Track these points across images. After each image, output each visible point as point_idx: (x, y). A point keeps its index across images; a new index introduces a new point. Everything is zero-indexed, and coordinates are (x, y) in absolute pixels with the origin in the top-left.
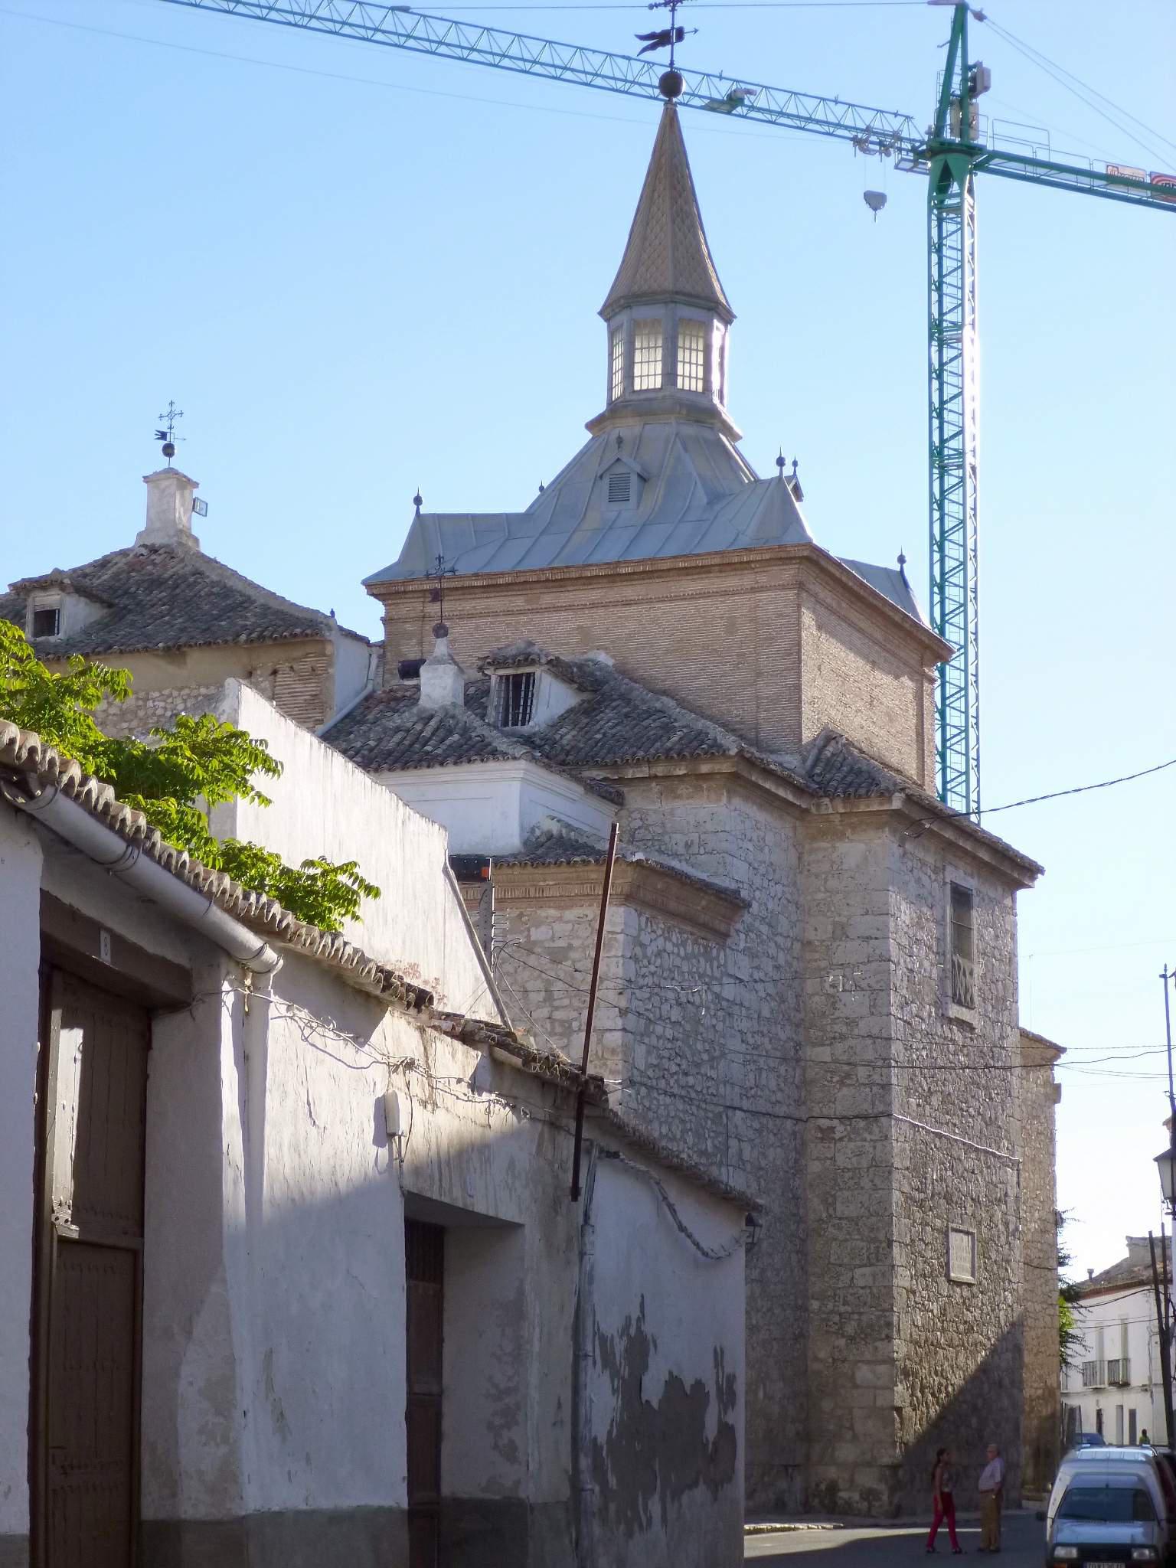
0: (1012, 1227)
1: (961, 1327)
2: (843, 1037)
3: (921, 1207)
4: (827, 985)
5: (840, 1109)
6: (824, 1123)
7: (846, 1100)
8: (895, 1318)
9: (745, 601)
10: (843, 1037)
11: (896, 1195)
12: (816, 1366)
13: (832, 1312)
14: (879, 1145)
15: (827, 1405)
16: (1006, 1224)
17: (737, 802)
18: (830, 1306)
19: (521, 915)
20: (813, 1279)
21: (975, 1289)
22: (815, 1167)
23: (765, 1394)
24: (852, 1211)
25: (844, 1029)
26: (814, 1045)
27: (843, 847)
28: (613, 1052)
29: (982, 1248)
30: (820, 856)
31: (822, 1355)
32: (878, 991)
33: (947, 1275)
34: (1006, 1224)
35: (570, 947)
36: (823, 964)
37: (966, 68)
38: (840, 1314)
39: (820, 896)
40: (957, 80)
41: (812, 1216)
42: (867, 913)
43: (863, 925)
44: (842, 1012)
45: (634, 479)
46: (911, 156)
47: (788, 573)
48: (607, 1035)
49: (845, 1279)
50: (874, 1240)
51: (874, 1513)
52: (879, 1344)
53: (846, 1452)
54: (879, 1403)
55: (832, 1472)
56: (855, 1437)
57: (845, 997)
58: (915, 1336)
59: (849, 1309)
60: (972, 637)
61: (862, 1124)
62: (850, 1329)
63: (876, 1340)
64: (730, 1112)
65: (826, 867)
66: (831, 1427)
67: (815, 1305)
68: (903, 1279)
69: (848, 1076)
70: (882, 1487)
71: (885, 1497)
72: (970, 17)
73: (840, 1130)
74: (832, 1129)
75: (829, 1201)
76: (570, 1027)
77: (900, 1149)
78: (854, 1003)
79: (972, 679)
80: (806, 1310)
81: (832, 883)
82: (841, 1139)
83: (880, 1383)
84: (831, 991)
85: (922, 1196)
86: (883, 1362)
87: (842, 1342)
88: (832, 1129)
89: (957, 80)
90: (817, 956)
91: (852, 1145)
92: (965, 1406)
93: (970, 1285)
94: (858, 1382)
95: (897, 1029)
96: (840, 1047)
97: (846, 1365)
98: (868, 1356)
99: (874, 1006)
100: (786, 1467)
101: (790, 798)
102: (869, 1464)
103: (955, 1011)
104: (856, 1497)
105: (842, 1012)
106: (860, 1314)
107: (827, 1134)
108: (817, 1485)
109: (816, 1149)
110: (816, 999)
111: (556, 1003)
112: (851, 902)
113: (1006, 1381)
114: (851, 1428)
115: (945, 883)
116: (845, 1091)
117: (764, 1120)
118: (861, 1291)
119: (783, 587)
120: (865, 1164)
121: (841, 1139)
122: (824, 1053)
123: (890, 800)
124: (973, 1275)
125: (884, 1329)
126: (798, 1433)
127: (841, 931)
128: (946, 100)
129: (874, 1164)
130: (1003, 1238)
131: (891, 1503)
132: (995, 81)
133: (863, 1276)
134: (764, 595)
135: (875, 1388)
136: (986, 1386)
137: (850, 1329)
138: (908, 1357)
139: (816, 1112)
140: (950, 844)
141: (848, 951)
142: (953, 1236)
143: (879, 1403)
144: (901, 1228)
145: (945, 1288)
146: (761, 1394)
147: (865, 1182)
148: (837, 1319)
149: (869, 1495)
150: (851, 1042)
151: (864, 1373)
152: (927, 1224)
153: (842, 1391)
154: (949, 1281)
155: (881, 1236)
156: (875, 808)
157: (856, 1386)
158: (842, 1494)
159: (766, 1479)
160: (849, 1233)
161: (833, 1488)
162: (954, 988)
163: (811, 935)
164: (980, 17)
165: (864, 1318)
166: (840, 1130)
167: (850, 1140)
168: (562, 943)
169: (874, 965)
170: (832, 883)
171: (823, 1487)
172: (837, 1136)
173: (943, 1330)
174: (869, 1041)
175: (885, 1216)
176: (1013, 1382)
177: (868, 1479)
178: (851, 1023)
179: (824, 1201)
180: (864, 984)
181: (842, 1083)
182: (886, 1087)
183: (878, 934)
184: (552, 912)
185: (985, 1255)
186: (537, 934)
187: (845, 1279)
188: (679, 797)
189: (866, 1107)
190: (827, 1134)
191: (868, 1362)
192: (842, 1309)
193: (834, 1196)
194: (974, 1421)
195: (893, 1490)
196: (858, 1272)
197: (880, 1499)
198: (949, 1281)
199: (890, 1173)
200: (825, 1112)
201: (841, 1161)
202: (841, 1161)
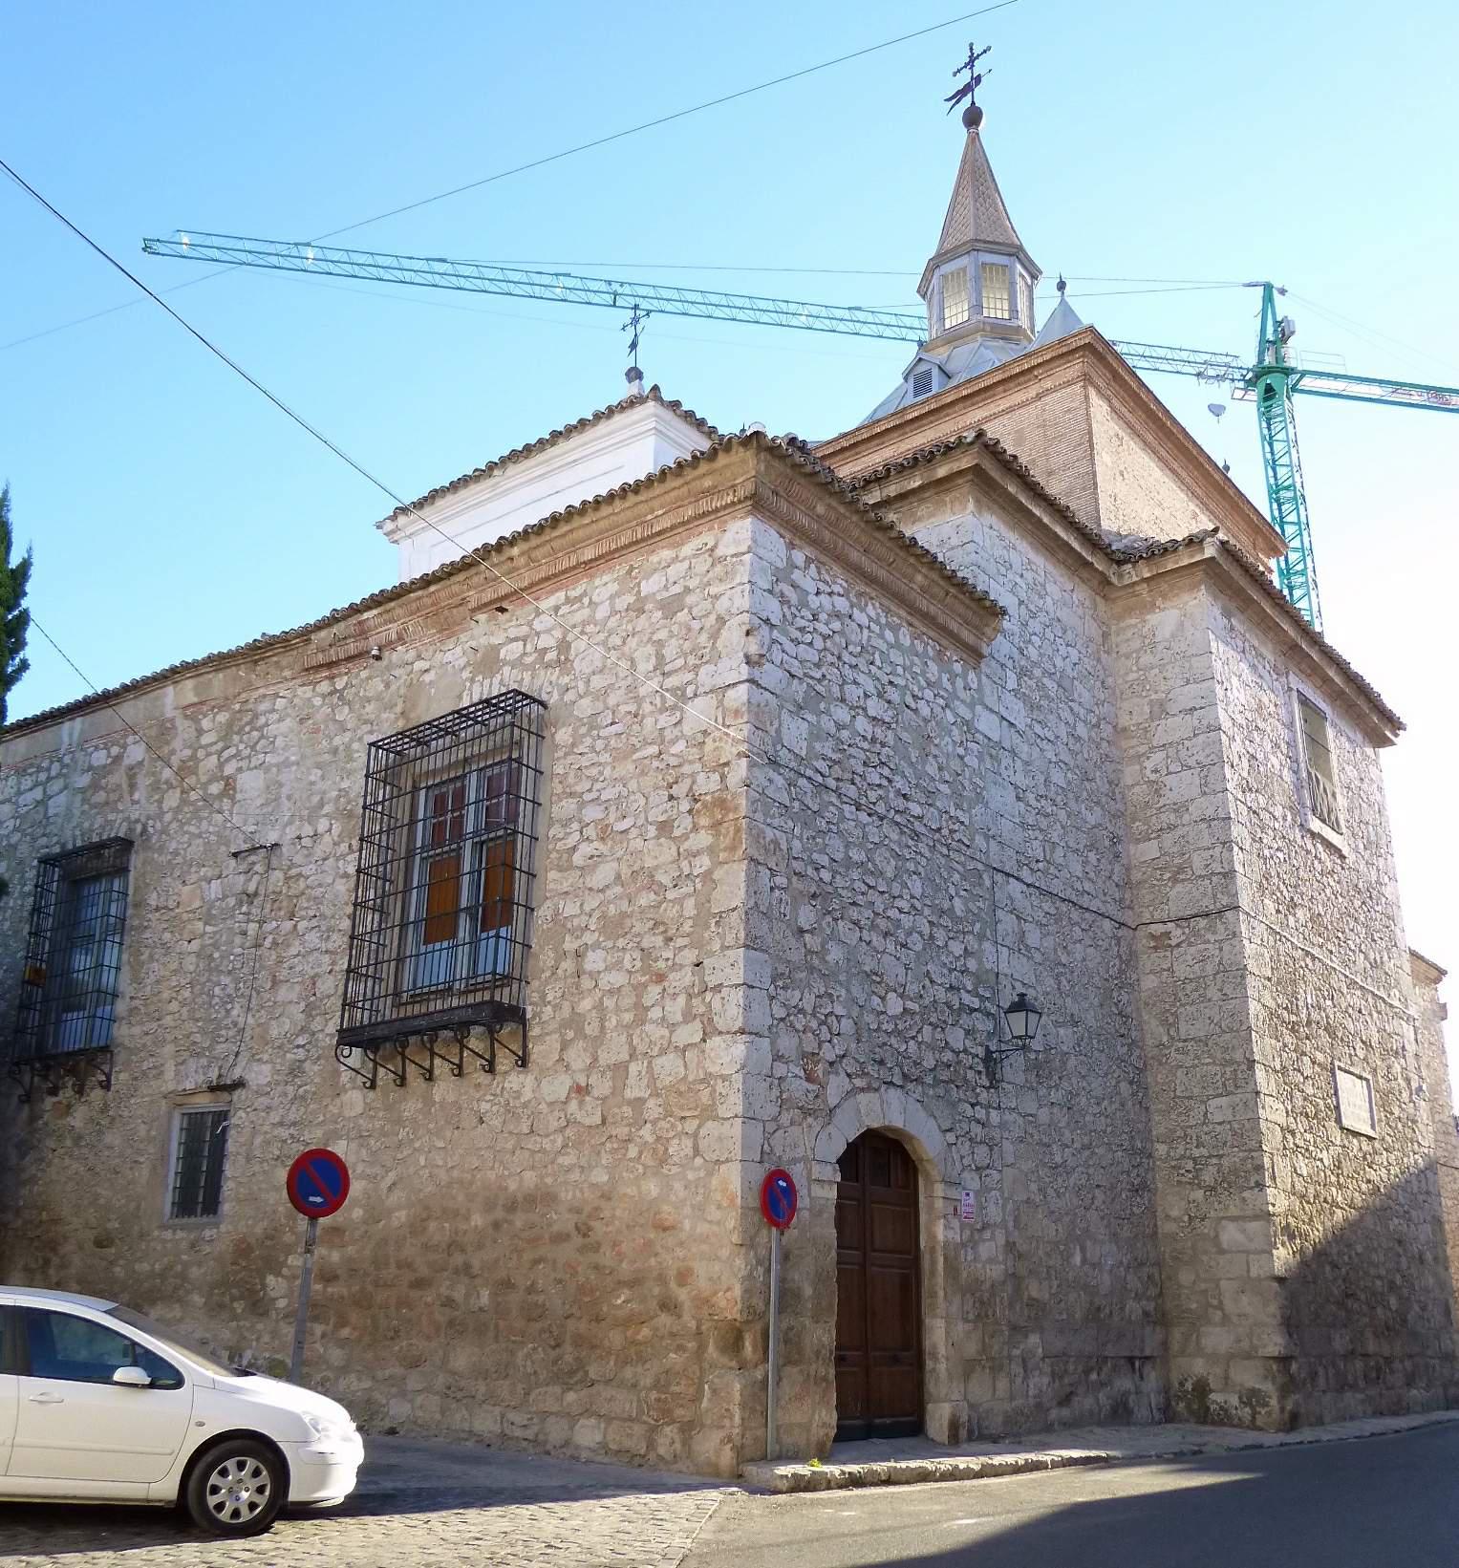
0: (1414, 1085)
1: (1364, 1187)
2: (1171, 827)
3: (1293, 1030)
4: (1148, 772)
5: (1174, 909)
6: (1157, 929)
7: (1180, 898)
8: (1266, 1160)
9: (1032, 410)
10: (1171, 827)
11: (1253, 1007)
12: (1169, 1227)
13: (1183, 1157)
14: (1226, 947)
15: (1185, 1277)
16: (1408, 1080)
17: (990, 519)
18: (1181, 1151)
19: (632, 568)
20: (1157, 1118)
21: (1377, 1145)
22: (1149, 983)
23: (1084, 1261)
24: (1199, 1030)
25: (1172, 817)
26: (1138, 841)
27: (1153, 619)
28: (737, 713)
29: (1382, 1100)
30: (1129, 634)
31: (1175, 1213)
32: (1210, 768)
33: (1339, 1120)
34: (1408, 1080)
35: (687, 590)
36: (1142, 749)
37: (1277, 323)
38: (1194, 1160)
39: (1133, 676)
40: (1270, 329)
41: (1150, 1042)
42: (1188, 682)
43: (1186, 696)
44: (1169, 797)
45: (935, 372)
46: (1241, 384)
47: (1075, 368)
48: (730, 693)
49: (1196, 1116)
50: (1231, 1062)
51: (1259, 1423)
52: (1246, 1194)
53: (1217, 1339)
54: (1254, 1273)
55: (1199, 1367)
56: (1226, 1319)
57: (1170, 781)
58: (1298, 1187)
59: (1204, 1152)
60: (1302, 526)
61: (1203, 923)
62: (1208, 1176)
63: (1243, 1189)
64: (999, 877)
65: (1136, 644)
66: (1194, 1306)
67: (1161, 1149)
68: (1273, 1112)
69: (1181, 869)
70: (1268, 1387)
71: (1274, 1402)
72: (1275, 293)
73: (1177, 934)
74: (1167, 935)
75: (1170, 1021)
76: (684, 694)
77: (1255, 950)
78: (1181, 786)
79: (1306, 552)
80: (1150, 1156)
81: (1146, 659)
82: (1178, 945)
83: (1252, 1246)
84: (1153, 777)
85: (1294, 1018)
86: (1256, 1218)
87: (1199, 1195)
88: (1167, 935)
89: (1270, 329)
90: (1134, 742)
91: (1192, 950)
92: (1378, 1283)
93: (1370, 1138)
94: (1225, 1246)
95: (1238, 811)
96: (1168, 839)
97: (1207, 1222)
98: (1233, 1211)
99: (1206, 784)
100: (1131, 1360)
101: (1076, 545)
102: (1248, 1356)
103: (1316, 825)
104: (1234, 1400)
105: (1169, 797)
106: (1220, 1157)
107: (1161, 942)
108: (1182, 1384)
109: (1149, 961)
110: (1136, 790)
111: (667, 669)
112: (1168, 675)
113: (1429, 1256)
114: (1220, 1307)
115: (1290, 689)
116: (1179, 887)
117: (1064, 907)
118: (1218, 1128)
119: (1069, 383)
120: (1210, 969)
121: (1178, 945)
122: (1150, 850)
123: (1202, 550)
124: (1373, 1127)
125: (1250, 1175)
126: (1146, 1314)
127: (1160, 710)
128: (1264, 344)
129: (1222, 970)
130: (1405, 1095)
131: (1282, 1409)
132: (1298, 328)
133: (1219, 1108)
134: (1047, 399)
135: (1248, 1252)
136: (1403, 1259)
137: (1208, 1176)
138: (1290, 1212)
139: (1146, 917)
140: (1295, 647)
141: (1174, 728)
142: (1339, 1075)
143: (1254, 1273)
144: (1263, 1047)
145: (1337, 1136)
146: (1077, 1259)
147: (1213, 993)
148: (1190, 1165)
149: (1252, 1398)
150: (1180, 831)
151: (1230, 1234)
152: (1304, 1054)
153: (1205, 1258)
154: (1342, 1128)
155: (1238, 1056)
156: (1186, 562)
157: (1222, 1252)
158: (1213, 1396)
159: (1094, 1376)
160: (1197, 1057)
161: (1202, 1389)
162: (1313, 798)
163: (1124, 721)
164: (1283, 292)
165: (1225, 1162)
166: (1177, 934)
167: (1190, 944)
168: (676, 589)
169: (1201, 738)
170: (1146, 659)
171: (1189, 1386)
172: (1173, 942)
173: (1340, 1186)
174: (1204, 826)
175: (1242, 1032)
176: (1436, 1259)
177: (1248, 1376)
178: (1180, 808)
179: (1164, 1022)
180: (1191, 762)
181: (1175, 880)
182: (1230, 875)
183: (1202, 703)
184: (666, 554)
185: (1385, 1106)
186: (648, 587)
187: (1196, 1116)
188: (920, 519)
189: (1207, 904)
190: (1161, 942)
191: (1234, 1219)
192: (1196, 1153)
193: (1175, 1015)
194: (1393, 1301)
195: (1284, 1392)
196: (1213, 1103)
197: (1266, 1405)
198: (1342, 1128)
199: (1243, 977)
200: (1157, 916)
201: (1181, 971)
202: (1181, 971)
